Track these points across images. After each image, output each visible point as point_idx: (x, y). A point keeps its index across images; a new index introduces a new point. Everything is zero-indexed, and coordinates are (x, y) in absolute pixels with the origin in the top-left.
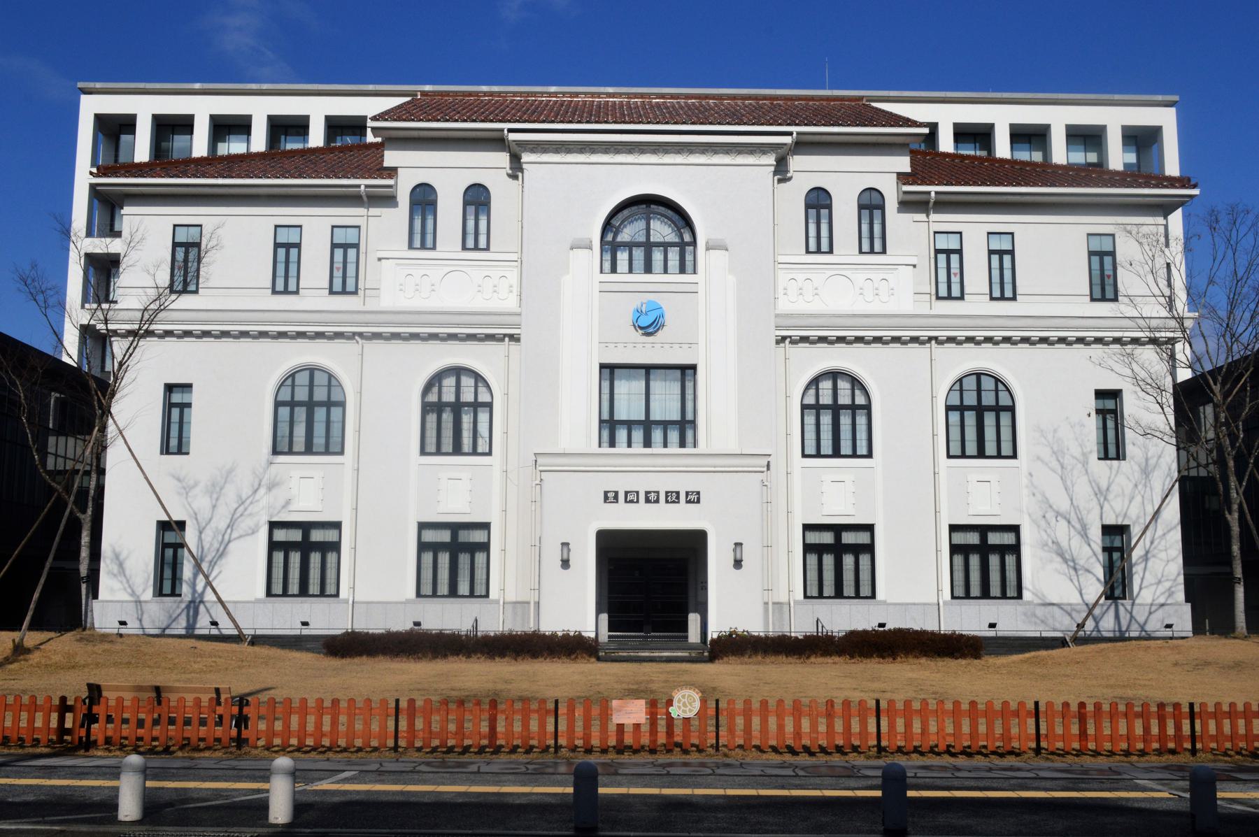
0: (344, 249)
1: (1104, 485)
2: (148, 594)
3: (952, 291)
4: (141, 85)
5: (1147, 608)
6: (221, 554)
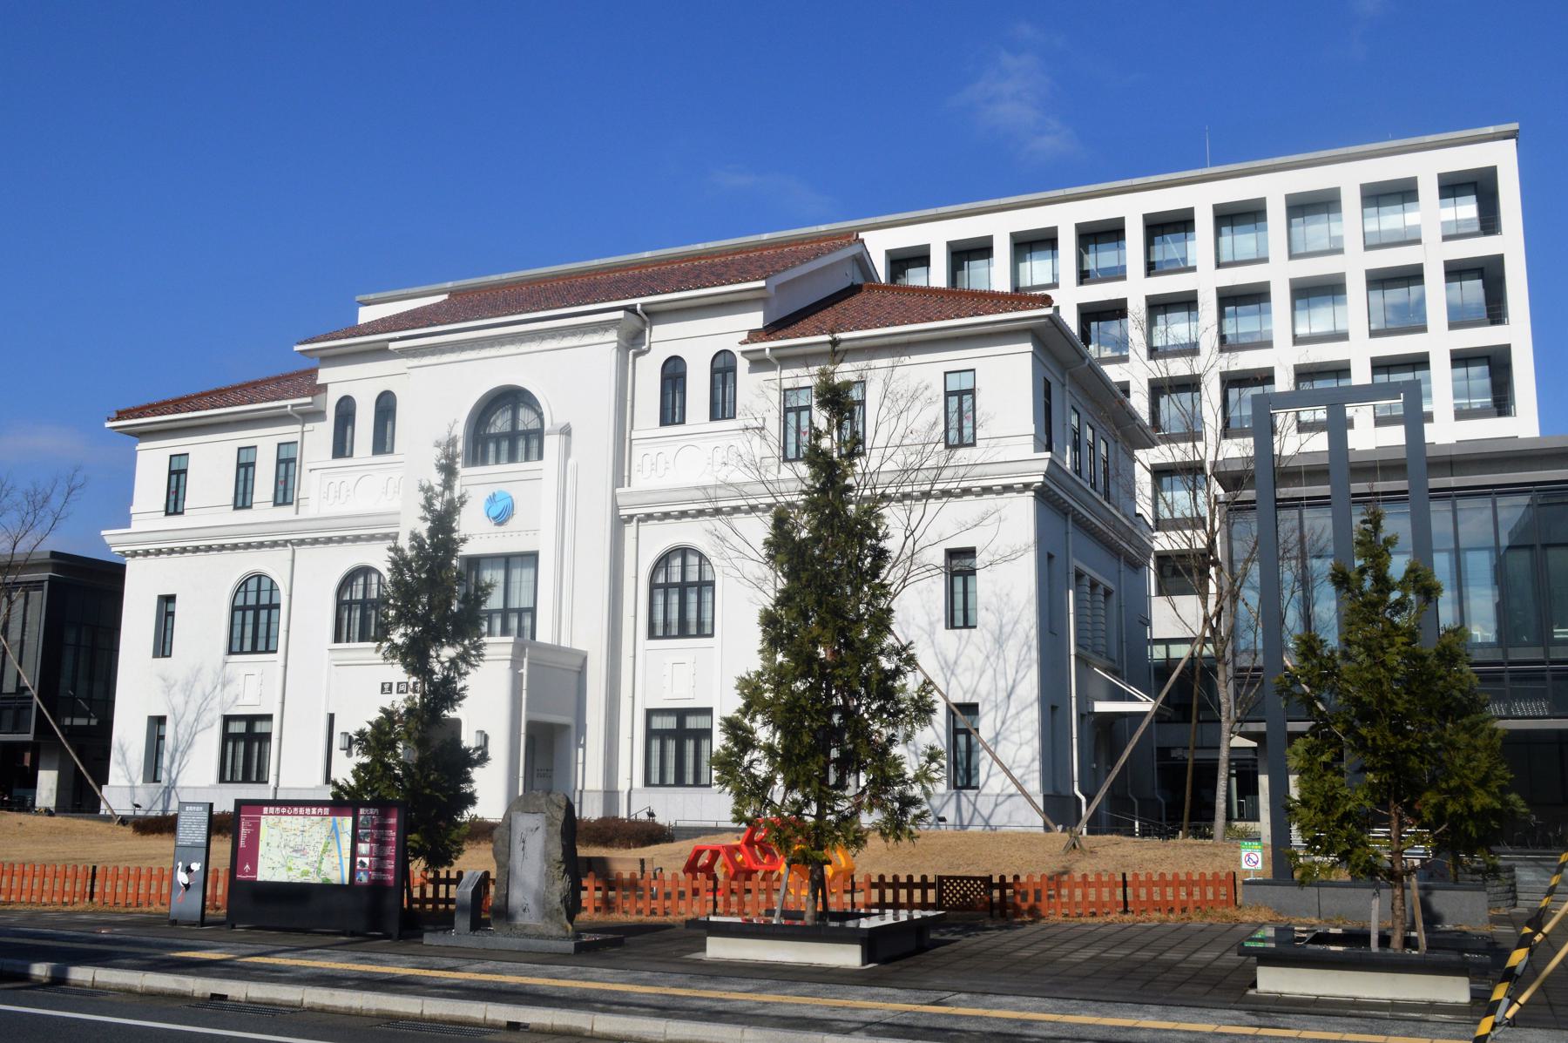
0: (286, 463)
1: (951, 657)
2: (139, 782)
3: (242, 500)
4: (404, 291)
5: (993, 800)
6: (190, 745)
